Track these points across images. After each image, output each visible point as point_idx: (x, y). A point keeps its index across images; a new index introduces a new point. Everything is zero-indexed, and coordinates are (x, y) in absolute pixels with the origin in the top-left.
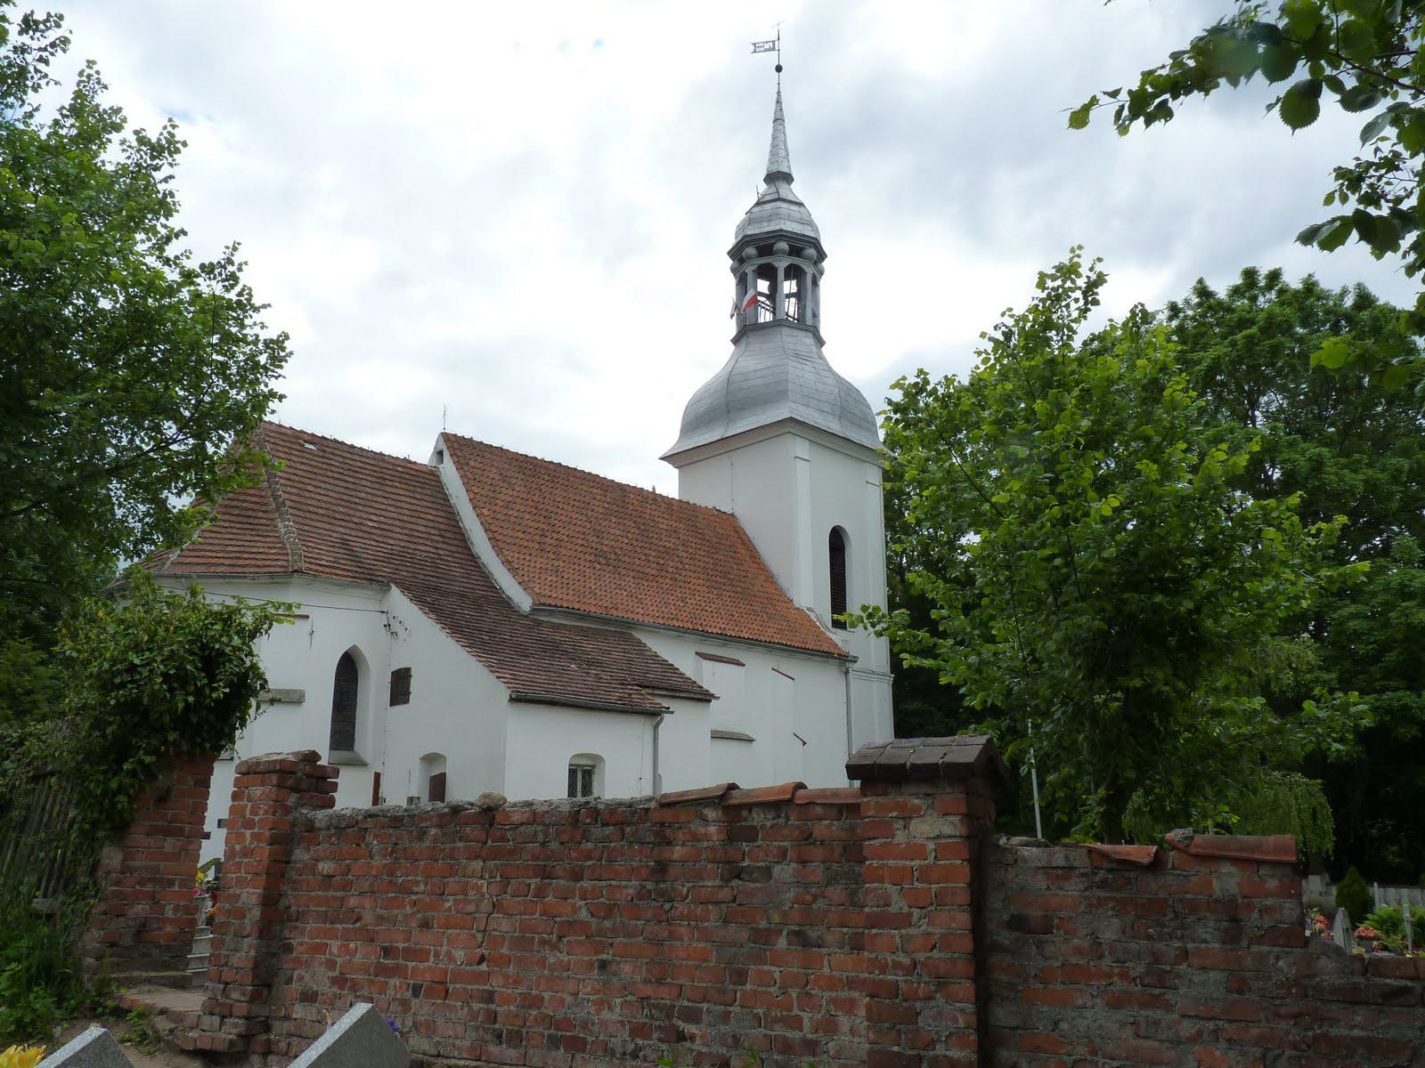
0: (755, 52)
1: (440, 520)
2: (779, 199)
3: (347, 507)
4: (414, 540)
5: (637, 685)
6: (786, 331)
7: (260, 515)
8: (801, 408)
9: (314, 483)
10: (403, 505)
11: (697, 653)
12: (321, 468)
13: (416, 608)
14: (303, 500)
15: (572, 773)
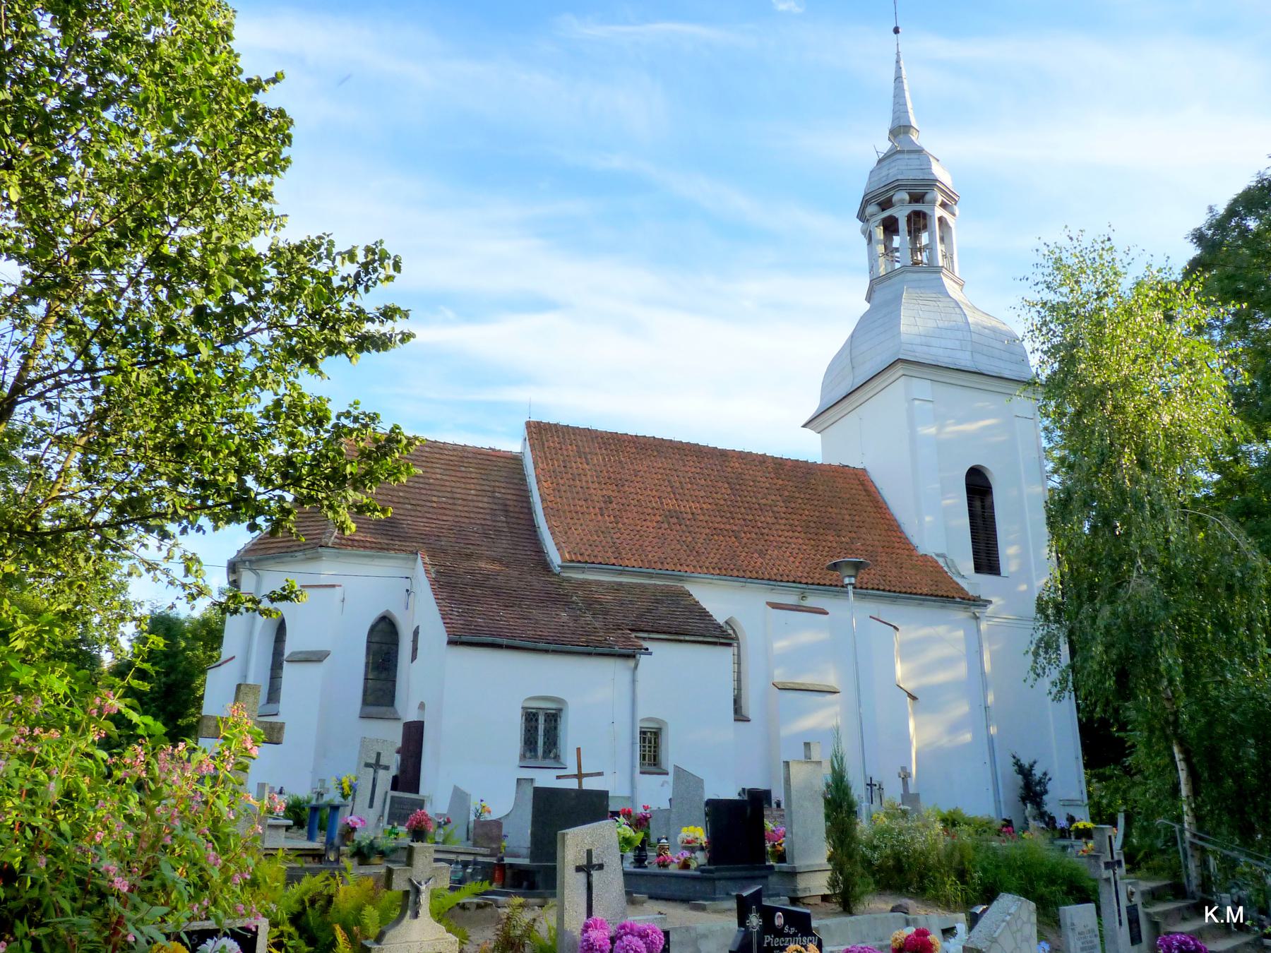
11: (768, 603)
15: (530, 717)
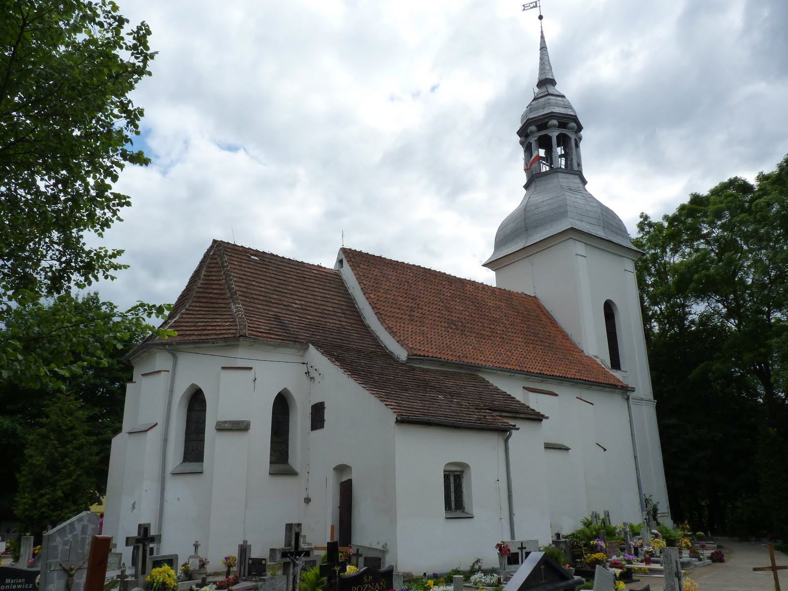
0: (524, 10)
1: (343, 303)
2: (549, 94)
3: (278, 295)
4: (325, 316)
5: (488, 409)
6: (560, 175)
7: (220, 301)
8: (577, 222)
9: (257, 280)
10: (317, 294)
11: (524, 388)
12: (261, 271)
13: (326, 359)
14: (248, 291)
15: (447, 477)
